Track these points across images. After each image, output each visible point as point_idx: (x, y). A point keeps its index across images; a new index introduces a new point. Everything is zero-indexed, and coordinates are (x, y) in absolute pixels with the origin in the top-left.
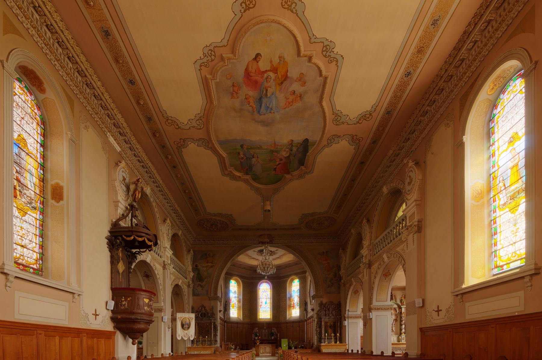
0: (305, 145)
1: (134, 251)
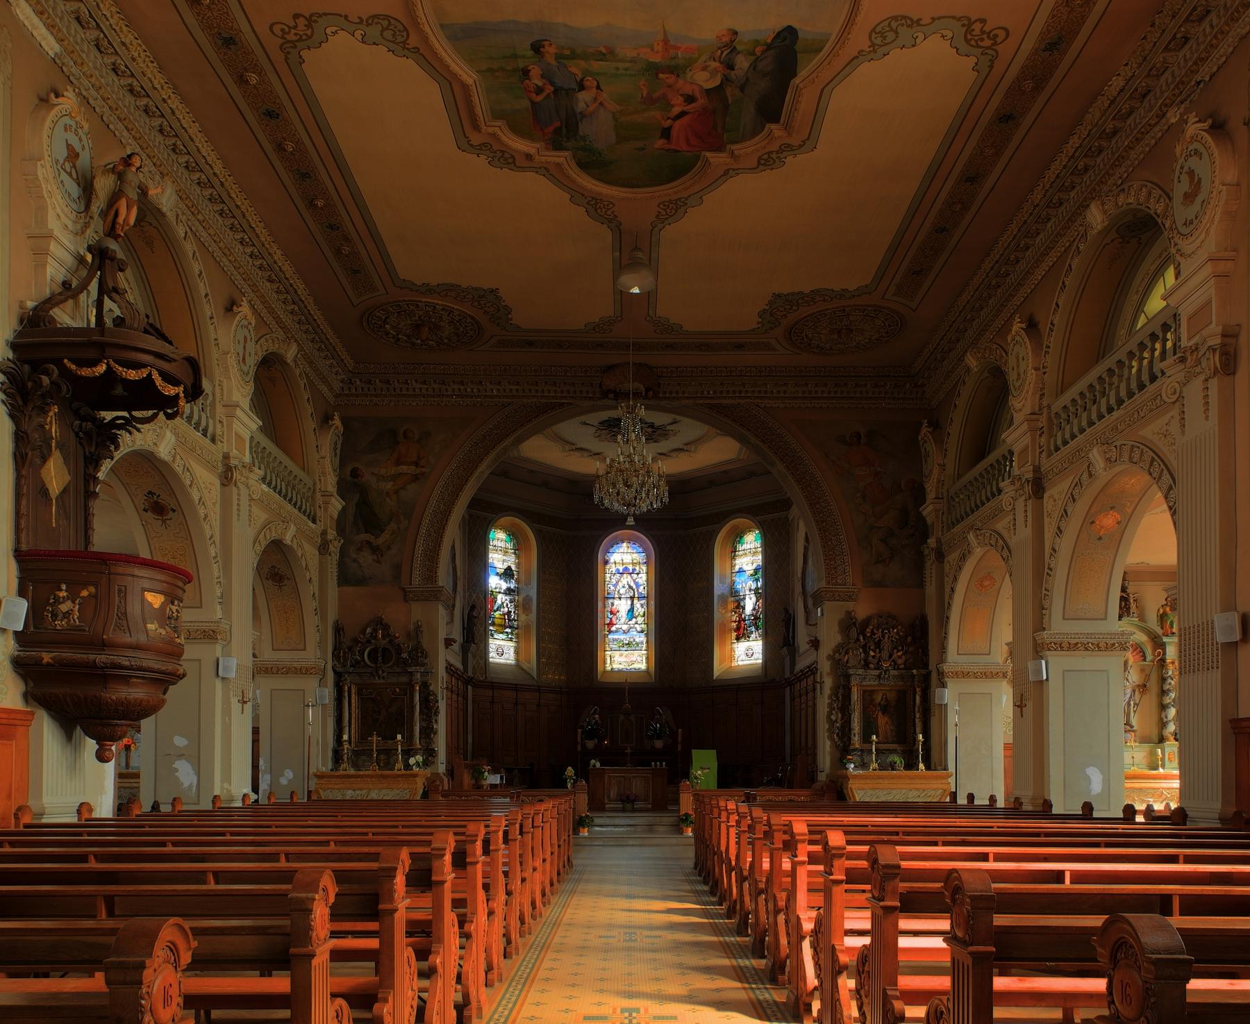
0: (785, 51)
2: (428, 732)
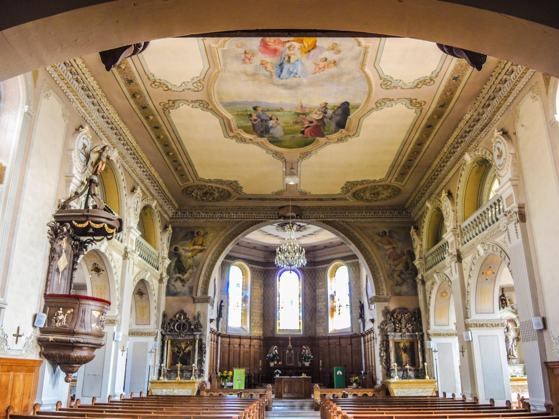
0: (345, 109)
1: (84, 239)
2: (201, 362)
